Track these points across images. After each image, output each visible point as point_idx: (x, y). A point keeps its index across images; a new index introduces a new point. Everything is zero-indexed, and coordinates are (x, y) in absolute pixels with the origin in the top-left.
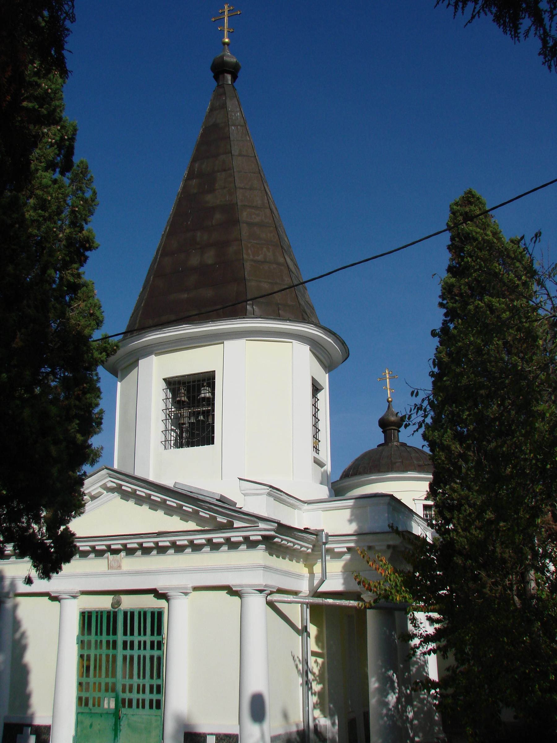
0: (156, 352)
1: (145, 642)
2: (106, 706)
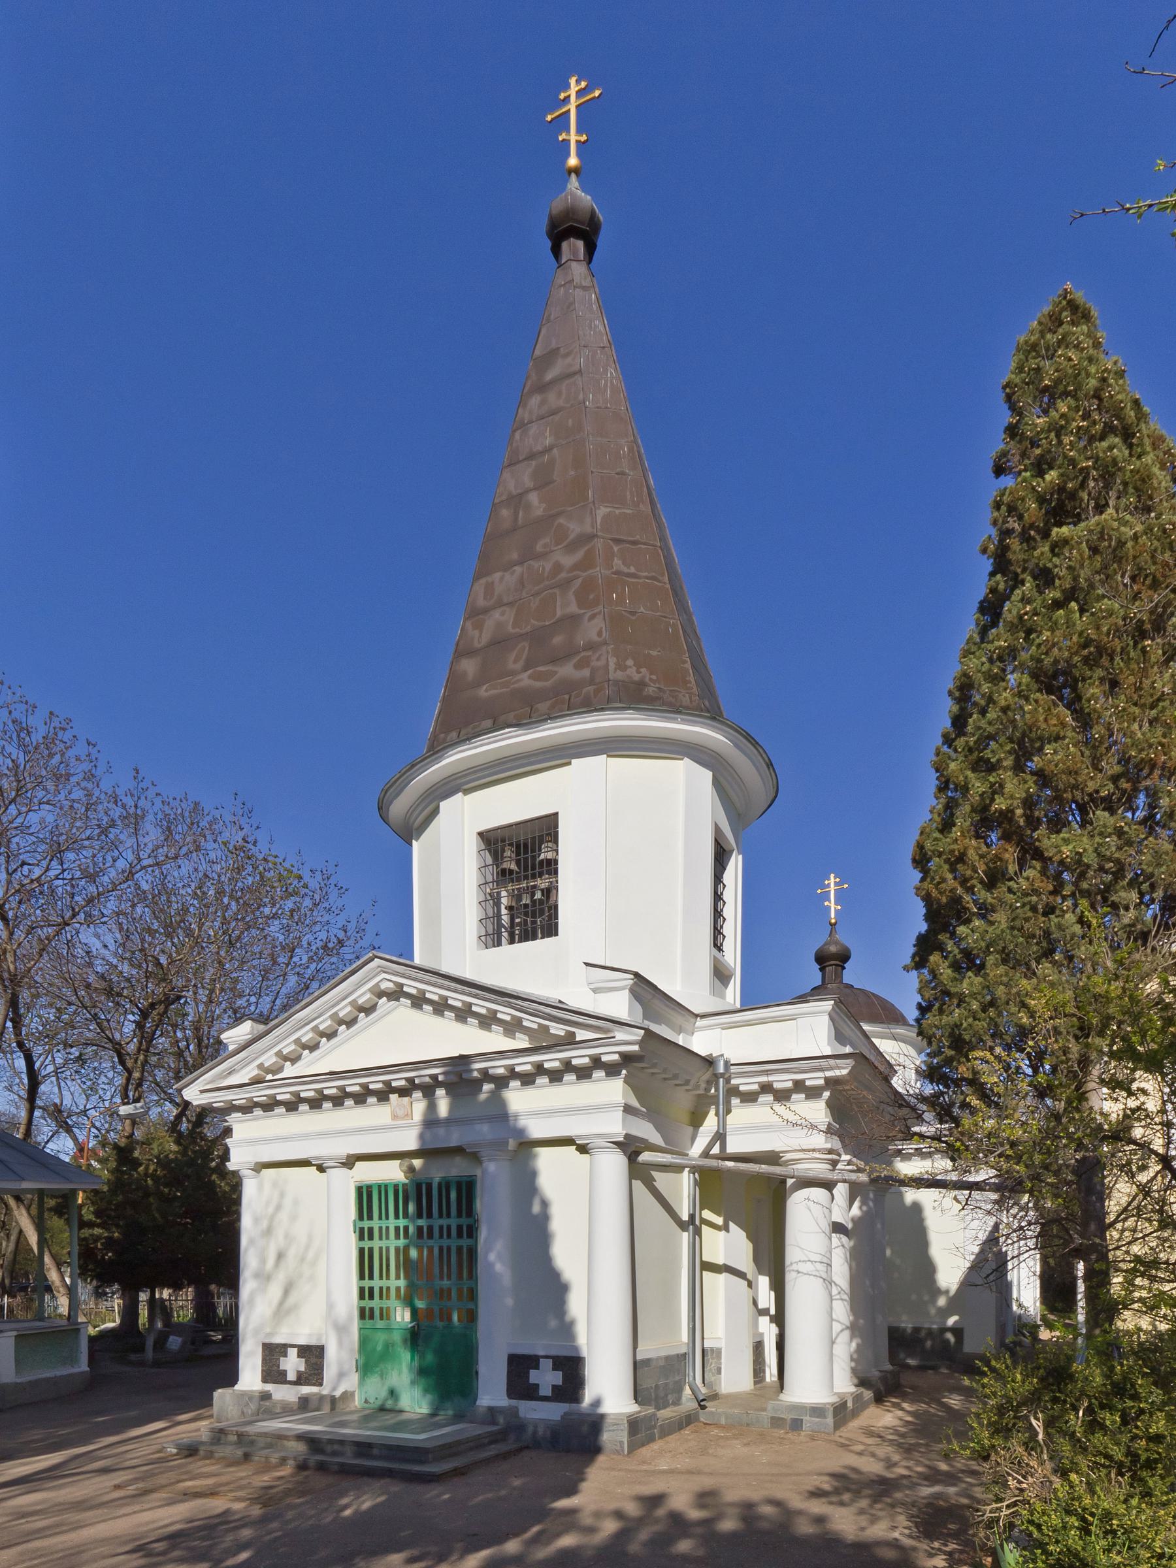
0: (466, 787)
1: (449, 1228)
2: (399, 1319)
